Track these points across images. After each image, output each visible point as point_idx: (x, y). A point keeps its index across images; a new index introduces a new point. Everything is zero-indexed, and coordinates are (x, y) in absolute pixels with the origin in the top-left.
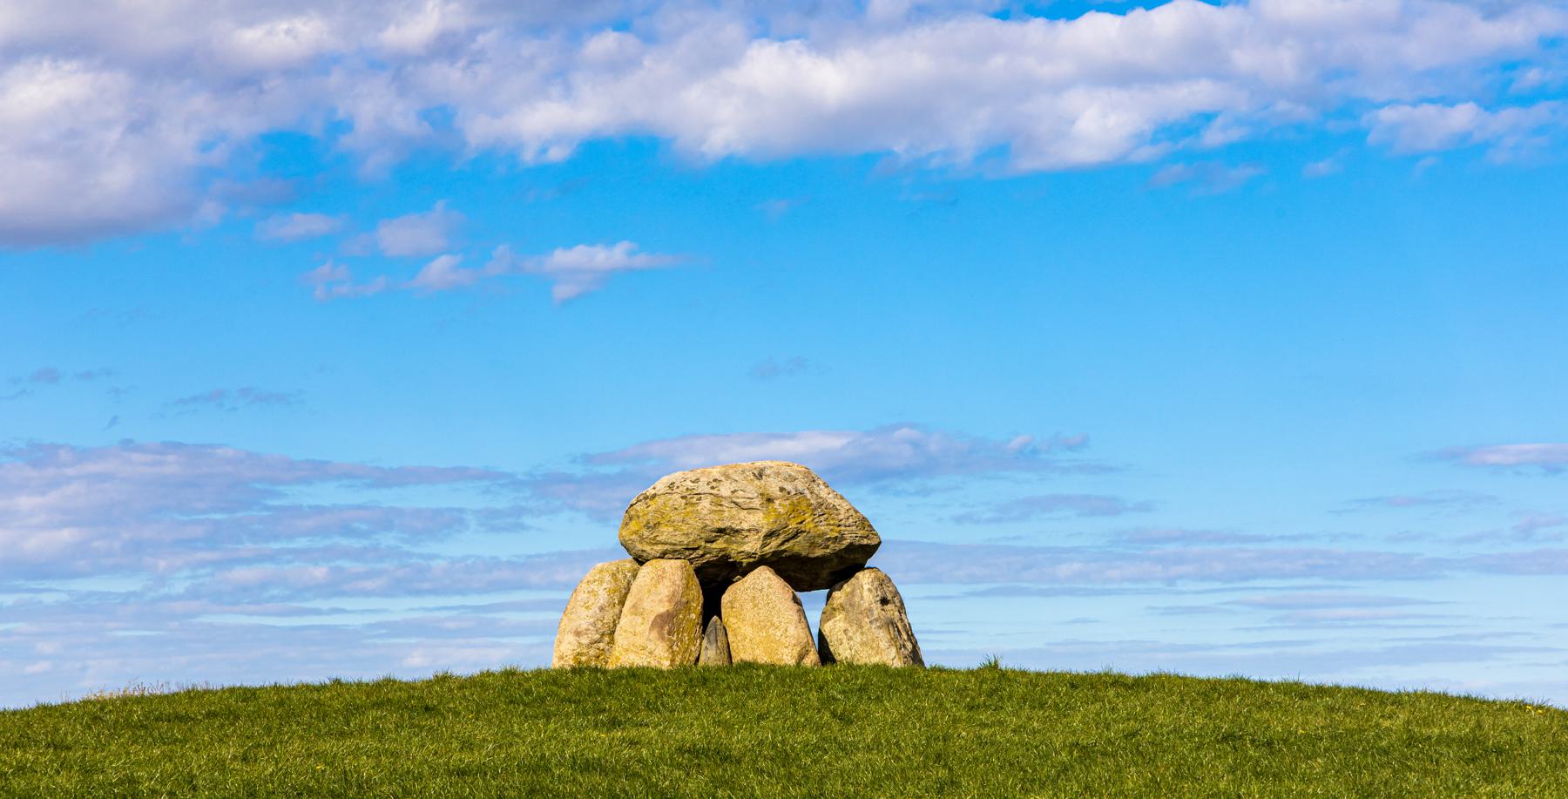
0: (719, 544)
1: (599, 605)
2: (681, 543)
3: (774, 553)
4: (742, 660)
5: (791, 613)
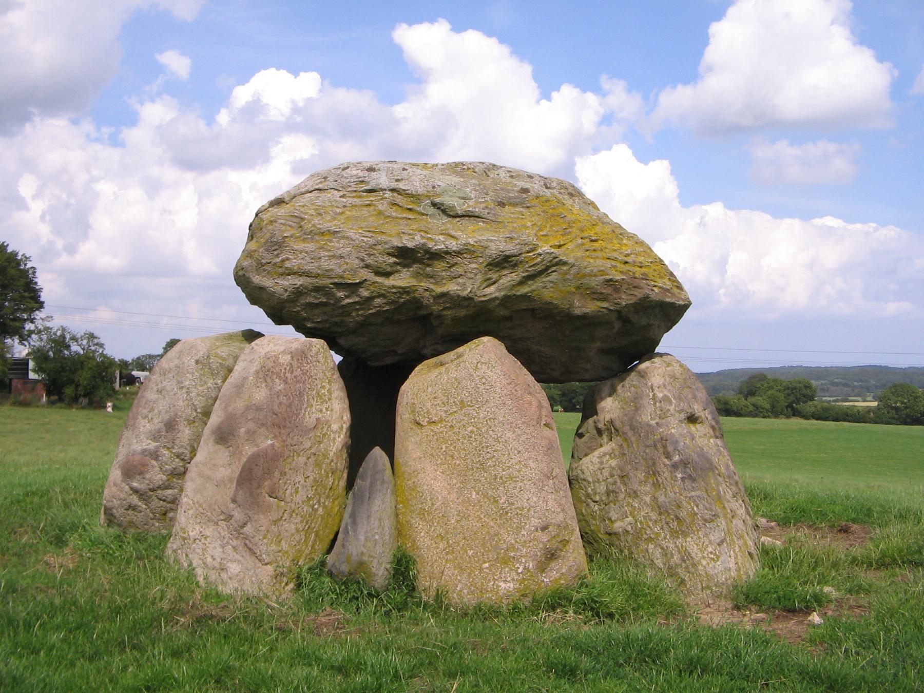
0: (403, 279)
1: (196, 358)
2: (327, 274)
3: (507, 301)
4: (546, 90)
5: (533, 454)
